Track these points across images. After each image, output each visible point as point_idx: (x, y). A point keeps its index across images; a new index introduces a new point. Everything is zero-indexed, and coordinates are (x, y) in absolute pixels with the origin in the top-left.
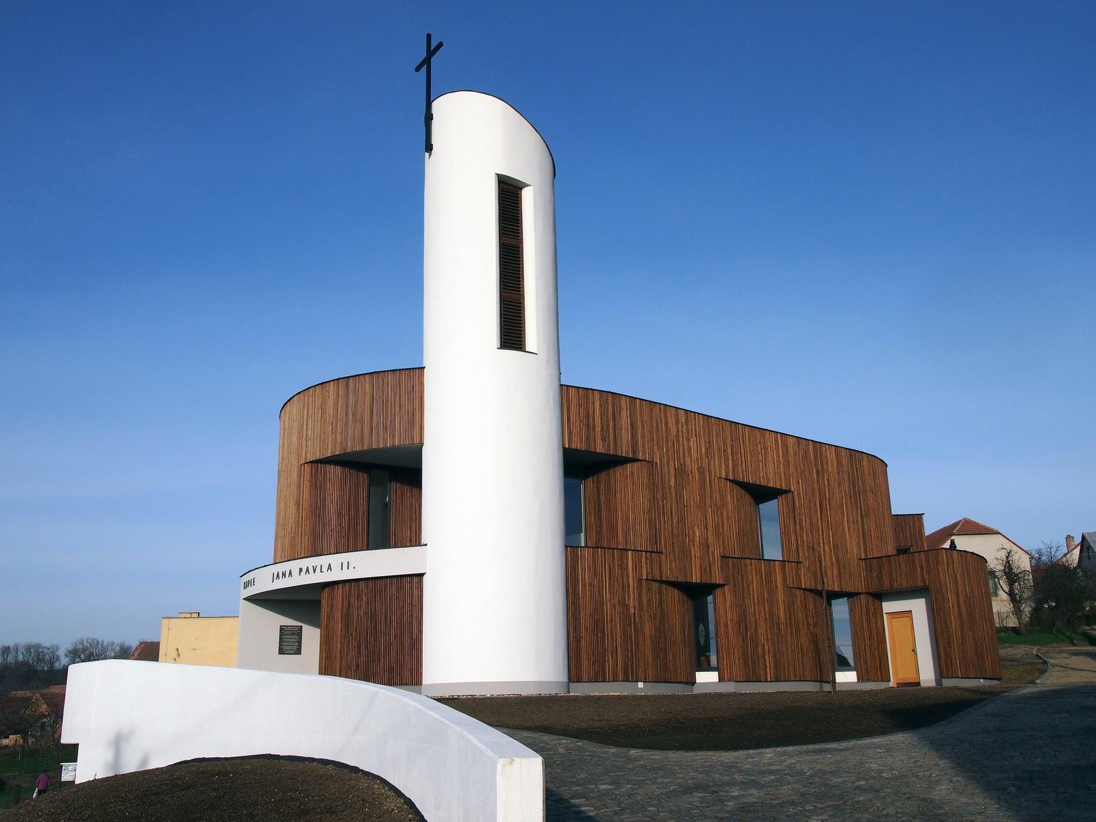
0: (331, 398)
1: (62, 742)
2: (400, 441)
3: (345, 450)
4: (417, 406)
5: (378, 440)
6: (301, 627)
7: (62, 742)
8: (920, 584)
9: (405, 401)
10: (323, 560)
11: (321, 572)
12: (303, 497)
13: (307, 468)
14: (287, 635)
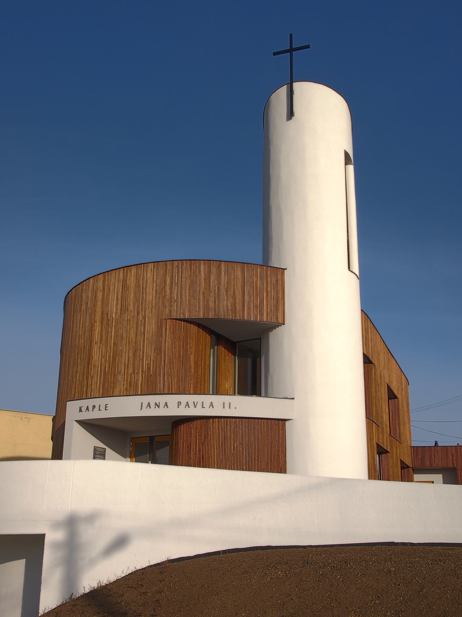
0: (202, 273)
1: (441, 475)
2: (267, 318)
3: (218, 315)
4: (280, 296)
5: (249, 314)
6: (105, 449)
7: (441, 475)
8: (451, 466)
9: (271, 290)
10: (161, 399)
11: (100, 410)
12: (165, 345)
13: (280, 321)
14: (98, 454)
